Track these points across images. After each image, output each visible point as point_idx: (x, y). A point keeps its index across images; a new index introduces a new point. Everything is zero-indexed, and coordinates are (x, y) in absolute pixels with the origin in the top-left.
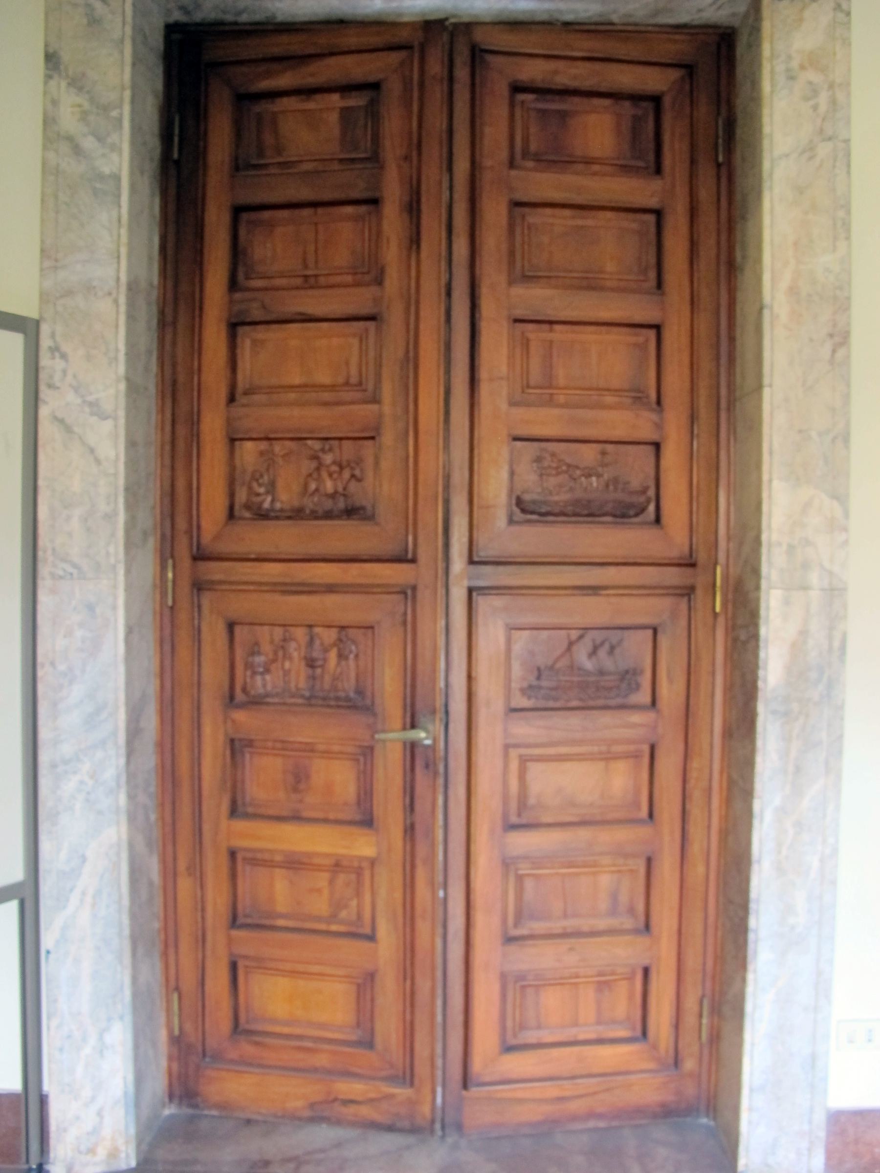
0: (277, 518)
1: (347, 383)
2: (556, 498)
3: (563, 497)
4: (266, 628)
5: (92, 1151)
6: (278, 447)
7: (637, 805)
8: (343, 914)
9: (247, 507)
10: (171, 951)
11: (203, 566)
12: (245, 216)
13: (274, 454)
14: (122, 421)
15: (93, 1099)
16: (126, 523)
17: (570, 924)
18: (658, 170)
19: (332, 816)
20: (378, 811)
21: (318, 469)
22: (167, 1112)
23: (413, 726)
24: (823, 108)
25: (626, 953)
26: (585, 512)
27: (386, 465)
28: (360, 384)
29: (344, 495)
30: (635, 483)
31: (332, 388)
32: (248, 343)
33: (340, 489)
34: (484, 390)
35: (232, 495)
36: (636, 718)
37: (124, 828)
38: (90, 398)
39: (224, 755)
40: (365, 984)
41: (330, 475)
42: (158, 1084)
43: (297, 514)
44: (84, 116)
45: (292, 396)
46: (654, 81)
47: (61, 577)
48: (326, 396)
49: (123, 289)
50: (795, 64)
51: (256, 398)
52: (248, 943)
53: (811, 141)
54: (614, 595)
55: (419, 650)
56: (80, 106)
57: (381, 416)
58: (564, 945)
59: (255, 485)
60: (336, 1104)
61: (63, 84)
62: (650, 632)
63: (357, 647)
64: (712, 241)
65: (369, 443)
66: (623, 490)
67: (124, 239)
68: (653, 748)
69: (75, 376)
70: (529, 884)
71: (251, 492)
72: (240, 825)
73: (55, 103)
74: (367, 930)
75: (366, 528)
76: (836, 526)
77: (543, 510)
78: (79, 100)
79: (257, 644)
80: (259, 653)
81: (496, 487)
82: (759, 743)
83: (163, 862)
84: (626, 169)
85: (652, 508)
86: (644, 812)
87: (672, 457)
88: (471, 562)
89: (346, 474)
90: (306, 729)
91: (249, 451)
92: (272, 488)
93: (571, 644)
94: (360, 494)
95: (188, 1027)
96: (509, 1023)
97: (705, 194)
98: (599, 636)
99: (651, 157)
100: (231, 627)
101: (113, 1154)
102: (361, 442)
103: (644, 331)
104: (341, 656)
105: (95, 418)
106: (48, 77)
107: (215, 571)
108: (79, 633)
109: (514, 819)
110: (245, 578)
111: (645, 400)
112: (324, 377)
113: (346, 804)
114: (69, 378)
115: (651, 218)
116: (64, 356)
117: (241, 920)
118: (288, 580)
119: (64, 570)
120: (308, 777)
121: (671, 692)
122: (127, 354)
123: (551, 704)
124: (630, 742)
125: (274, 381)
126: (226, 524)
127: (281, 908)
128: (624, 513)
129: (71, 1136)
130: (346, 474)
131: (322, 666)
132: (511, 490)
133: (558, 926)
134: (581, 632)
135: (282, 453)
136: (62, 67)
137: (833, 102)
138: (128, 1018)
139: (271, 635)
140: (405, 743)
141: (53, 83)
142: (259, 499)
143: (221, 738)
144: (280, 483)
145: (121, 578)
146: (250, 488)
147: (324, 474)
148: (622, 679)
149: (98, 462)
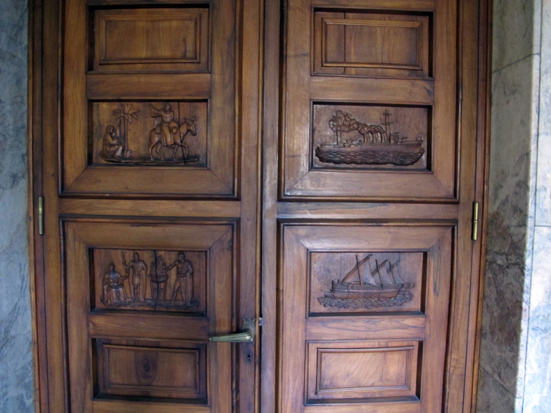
0: (127, 164)
1: (184, 57)
2: (348, 149)
3: (354, 148)
4: (119, 252)
6: (128, 108)
7: (407, 384)
9: (103, 155)
11: (68, 202)
13: (124, 113)
21: (160, 126)
26: (369, 161)
27: (216, 122)
29: (182, 146)
30: (411, 138)
31: (172, 60)
32: (103, 24)
33: (178, 141)
34: (291, 63)
35: (90, 145)
36: (409, 321)
39: (88, 350)
41: (171, 130)
43: (143, 162)
45: (139, 67)
51: (111, 68)
54: (394, 226)
55: (243, 268)
57: (211, 83)
59: (109, 138)
65: (202, 105)
68: (421, 344)
71: (106, 143)
75: (200, 173)
77: (337, 159)
79: (113, 264)
80: (114, 271)
81: (299, 141)
85: (424, 157)
86: (413, 392)
87: (442, 119)
88: (280, 199)
89: (183, 130)
91: (104, 111)
92: (123, 141)
93: (358, 264)
98: (381, 258)
100: (91, 252)
102: (195, 104)
103: (420, 18)
107: (79, 207)
109: (312, 395)
110: (101, 212)
111: (419, 72)
112: (165, 52)
118: (137, 214)
120: (155, 367)
121: (436, 302)
123: (342, 310)
124: (402, 339)
126: (86, 168)
128: (402, 162)
130: (183, 130)
131: (165, 281)
132: (312, 142)
134: (367, 254)
135: (130, 112)
139: (123, 257)
140: (232, 344)
142: (113, 149)
143: (85, 338)
144: (130, 136)
146: (105, 140)
147: (167, 131)
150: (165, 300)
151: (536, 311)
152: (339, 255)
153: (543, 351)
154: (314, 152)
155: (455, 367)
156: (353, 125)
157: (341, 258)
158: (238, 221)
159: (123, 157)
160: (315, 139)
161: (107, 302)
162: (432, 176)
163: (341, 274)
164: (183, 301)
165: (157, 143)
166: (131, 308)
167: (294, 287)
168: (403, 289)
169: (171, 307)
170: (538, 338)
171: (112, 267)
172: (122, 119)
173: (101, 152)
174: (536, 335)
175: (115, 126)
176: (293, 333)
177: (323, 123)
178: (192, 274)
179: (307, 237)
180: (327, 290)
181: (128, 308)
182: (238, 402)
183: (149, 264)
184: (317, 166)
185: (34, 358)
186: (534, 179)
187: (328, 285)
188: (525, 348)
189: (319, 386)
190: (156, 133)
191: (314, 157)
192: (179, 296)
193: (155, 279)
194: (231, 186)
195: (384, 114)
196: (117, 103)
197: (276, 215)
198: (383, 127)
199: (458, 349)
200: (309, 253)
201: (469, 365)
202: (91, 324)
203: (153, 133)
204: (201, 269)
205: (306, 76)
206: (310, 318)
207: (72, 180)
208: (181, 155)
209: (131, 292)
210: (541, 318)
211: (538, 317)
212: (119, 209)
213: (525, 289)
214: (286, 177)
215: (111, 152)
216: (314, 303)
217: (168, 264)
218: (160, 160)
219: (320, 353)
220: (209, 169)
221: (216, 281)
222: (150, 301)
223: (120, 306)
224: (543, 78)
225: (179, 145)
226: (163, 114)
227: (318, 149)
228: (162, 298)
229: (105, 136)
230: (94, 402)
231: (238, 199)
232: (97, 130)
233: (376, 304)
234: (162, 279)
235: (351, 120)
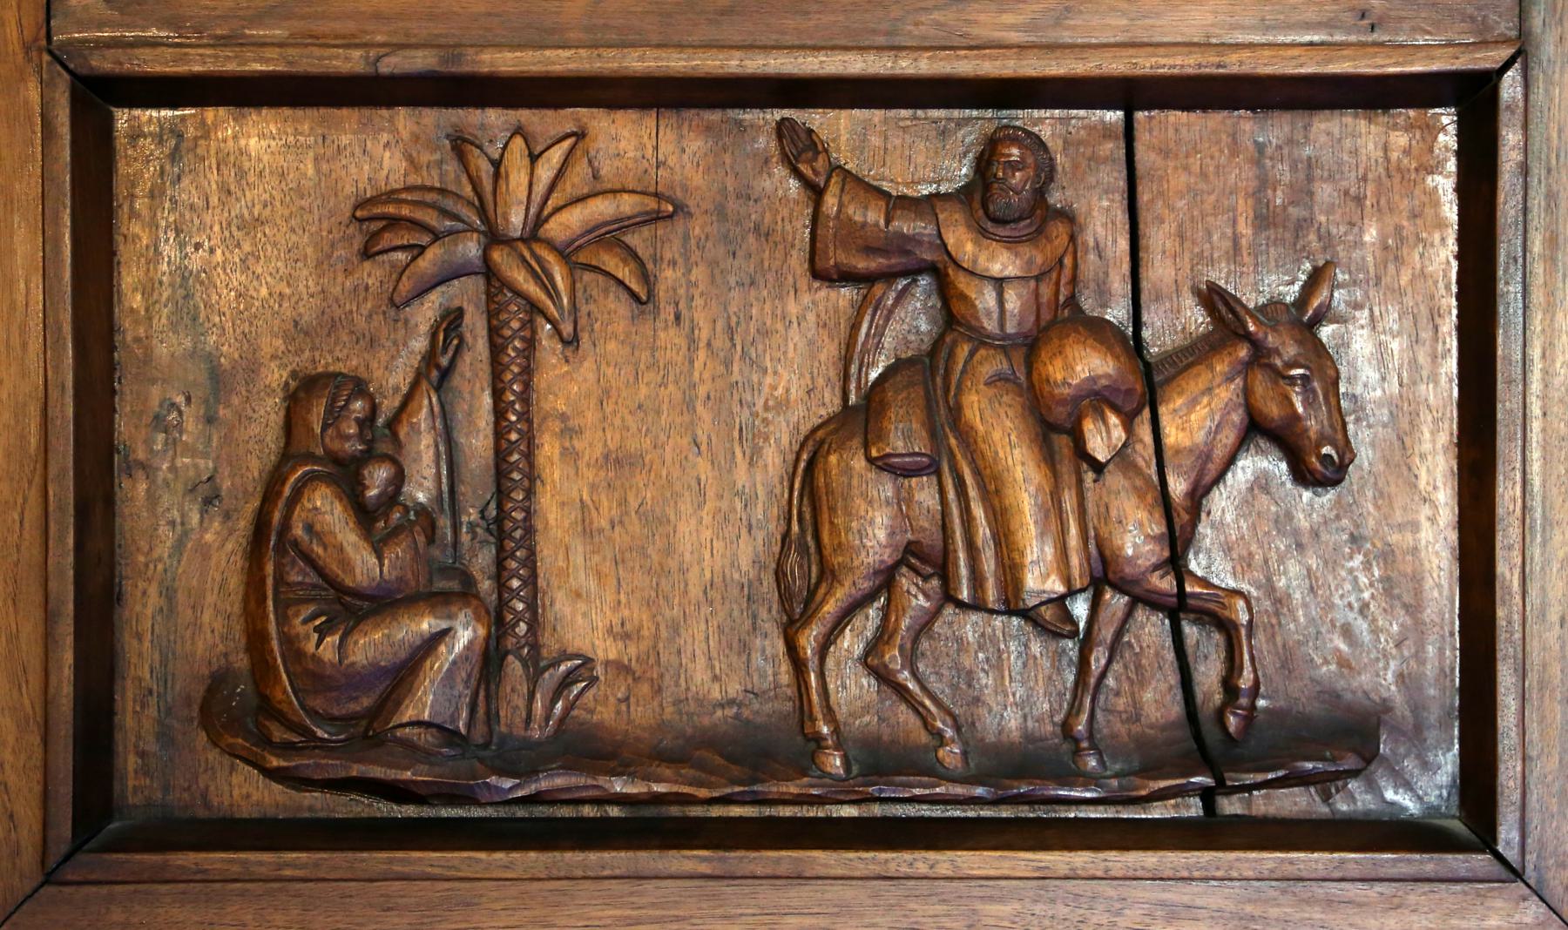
6: (526, 169)
13: (494, 237)
29: (1177, 608)
41: (1056, 430)
89: (1194, 417)
92: (488, 553)
135: (567, 223)
142: (372, 645)
146: (267, 538)
159: (478, 745)
165: (886, 580)
172: (467, 293)
173: (219, 681)
175: (393, 375)
190: (882, 464)
196: (404, 119)
203: (849, 465)
215: (356, 680)
218: (937, 772)
226: (962, 241)
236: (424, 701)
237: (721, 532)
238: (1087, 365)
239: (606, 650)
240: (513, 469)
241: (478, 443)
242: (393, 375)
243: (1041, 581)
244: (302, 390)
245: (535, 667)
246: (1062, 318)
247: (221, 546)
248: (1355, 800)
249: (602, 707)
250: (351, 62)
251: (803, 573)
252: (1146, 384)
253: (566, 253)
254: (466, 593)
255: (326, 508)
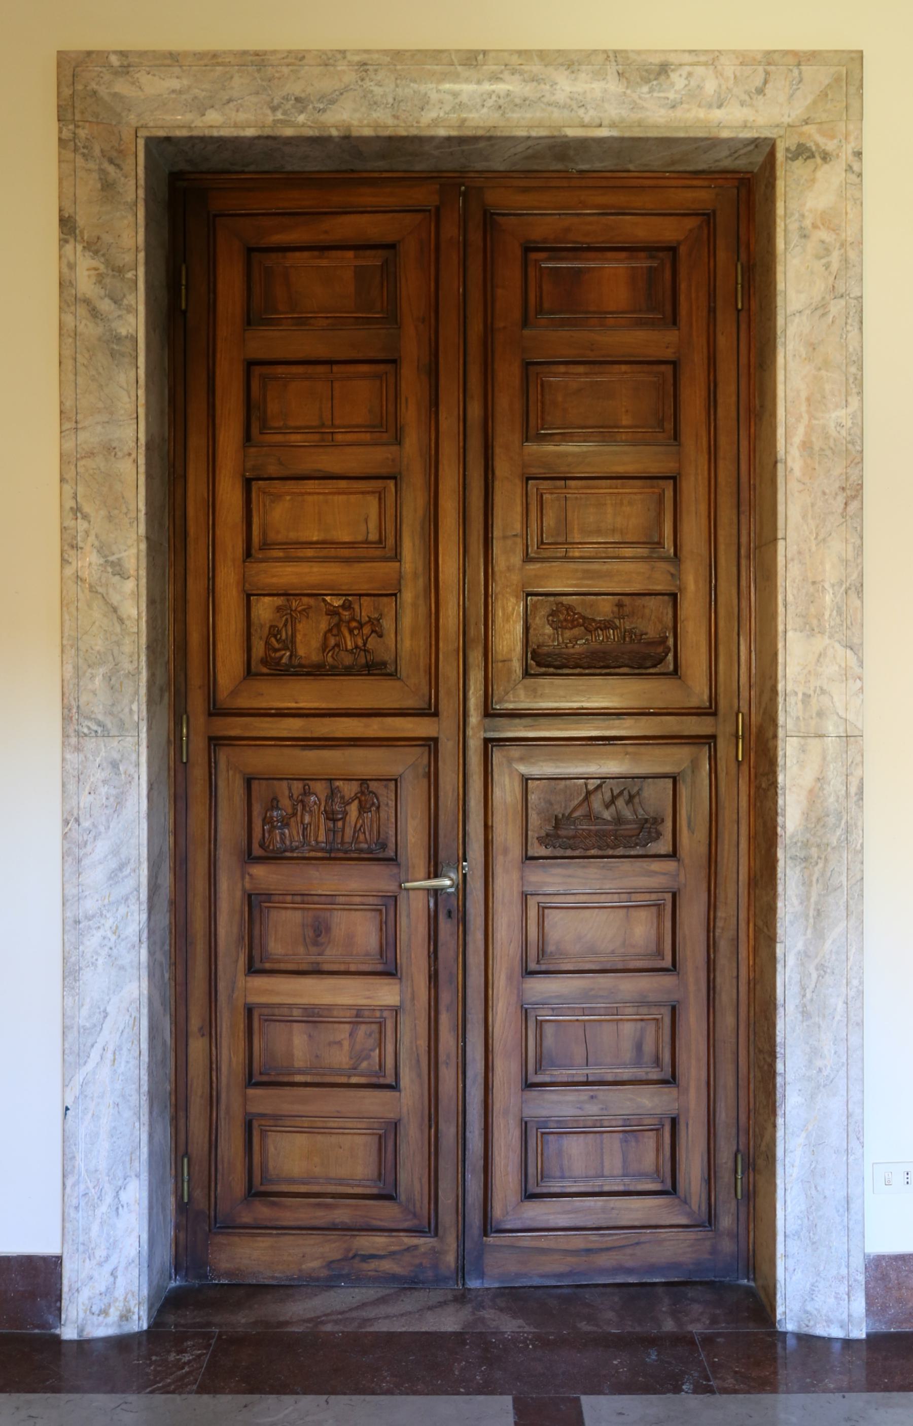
2: (572, 651)
5: (104, 1312)
8: (364, 1065)
10: (182, 1114)
12: (257, 371)
13: (291, 610)
14: (143, 581)
15: (107, 1258)
16: (148, 681)
17: (594, 1073)
18: (675, 322)
19: (353, 968)
20: (402, 959)
22: (173, 1284)
23: (436, 876)
24: (835, 266)
25: (650, 1102)
28: (380, 541)
29: (365, 650)
31: (351, 545)
34: (498, 548)
36: (656, 866)
37: (145, 984)
38: (111, 558)
40: (388, 1134)
41: (351, 631)
42: (166, 1254)
43: (316, 671)
44: (100, 279)
45: (310, 553)
46: (669, 231)
47: (86, 735)
48: (346, 553)
49: (142, 450)
50: (808, 223)
52: (264, 1101)
53: (823, 298)
56: (96, 269)
58: (584, 1093)
60: (356, 1260)
61: (79, 248)
62: (669, 783)
63: (378, 800)
64: (733, 388)
66: (639, 642)
67: (142, 400)
69: (97, 536)
70: (549, 1030)
72: (259, 982)
73: (72, 266)
74: (390, 1080)
75: (387, 684)
76: (852, 675)
77: (556, 663)
78: (95, 263)
80: (278, 808)
81: (509, 637)
82: (780, 889)
83: (175, 1023)
84: (640, 323)
85: (670, 657)
89: (366, 630)
90: (327, 880)
92: (290, 644)
93: (589, 793)
94: (381, 648)
95: (198, 1193)
96: (531, 1170)
97: (724, 342)
99: (668, 308)
100: (249, 782)
101: (125, 1317)
104: (362, 809)
105: (117, 577)
106: (63, 242)
107: (235, 727)
108: (103, 790)
113: (367, 954)
114: (92, 538)
115: (668, 369)
116: (85, 517)
117: (257, 1078)
119: (89, 728)
120: (328, 929)
121: (693, 842)
122: (146, 514)
123: (569, 853)
125: (293, 536)
126: (244, 679)
127: (299, 1064)
129: (85, 1294)
133: (579, 1074)
135: (299, 609)
136: (77, 231)
137: (845, 260)
138: (145, 1176)
139: (290, 789)
141: (69, 248)
142: (278, 654)
143: (239, 894)
145: (144, 735)
146: (267, 643)
148: (641, 829)
149: (121, 620)
150: (342, 843)
151: (792, 836)
152: (563, 782)
153: (804, 884)
154: (529, 655)
155: (723, 929)
156: (577, 619)
157: (566, 786)
158: (435, 740)
159: (290, 665)
160: (530, 638)
161: (269, 846)
162: (679, 681)
163: (566, 808)
164: (366, 842)
165: (333, 648)
166: (300, 855)
167: (507, 824)
168: (648, 828)
169: (351, 850)
170: (798, 869)
171: (275, 802)
172: (289, 616)
174: (796, 866)
175: (281, 625)
176: (506, 884)
177: (540, 619)
178: (378, 808)
179: (522, 759)
180: (549, 828)
181: (295, 855)
182: (436, 972)
183: (323, 798)
184: (533, 672)
185: (170, 923)
186: (783, 682)
187: (549, 820)
188: (783, 881)
189: (542, 952)
191: (529, 661)
192: (362, 837)
193: (331, 816)
194: (427, 698)
195: (617, 605)
196: (282, 598)
197: (482, 733)
198: (617, 622)
199: (726, 903)
200: (526, 780)
201: (743, 925)
202: (247, 876)
204: (390, 802)
205: (517, 437)
206: (528, 862)
207: (225, 694)
208: (363, 661)
209: (298, 833)
210: (799, 844)
211: (796, 843)
212: (285, 729)
213: (779, 811)
214: (495, 687)
216: (532, 844)
217: (347, 798)
219: (542, 910)
220: (399, 679)
221: (409, 815)
222: (323, 845)
223: (285, 851)
224: (789, 566)
225: (361, 650)
226: (341, 611)
227: (534, 652)
228: (339, 841)
229: (268, 638)
230: (249, 979)
231: (436, 714)
232: (256, 630)
233: (611, 844)
234: (340, 816)
235: (575, 614)
236: (284, 661)
237: (316, 642)
238: (354, 624)
239: (303, 655)
240: (294, 636)
241: (290, 633)
242: (281, 625)
243: (349, 647)
244: (271, 627)
245: (296, 656)
246: (353, 619)
247: (262, 644)
248: (384, 671)
249: (303, 662)
250: (275, 592)
251: (324, 647)
252: (361, 626)
253: (299, 612)
254: (288, 649)
255: (273, 640)
